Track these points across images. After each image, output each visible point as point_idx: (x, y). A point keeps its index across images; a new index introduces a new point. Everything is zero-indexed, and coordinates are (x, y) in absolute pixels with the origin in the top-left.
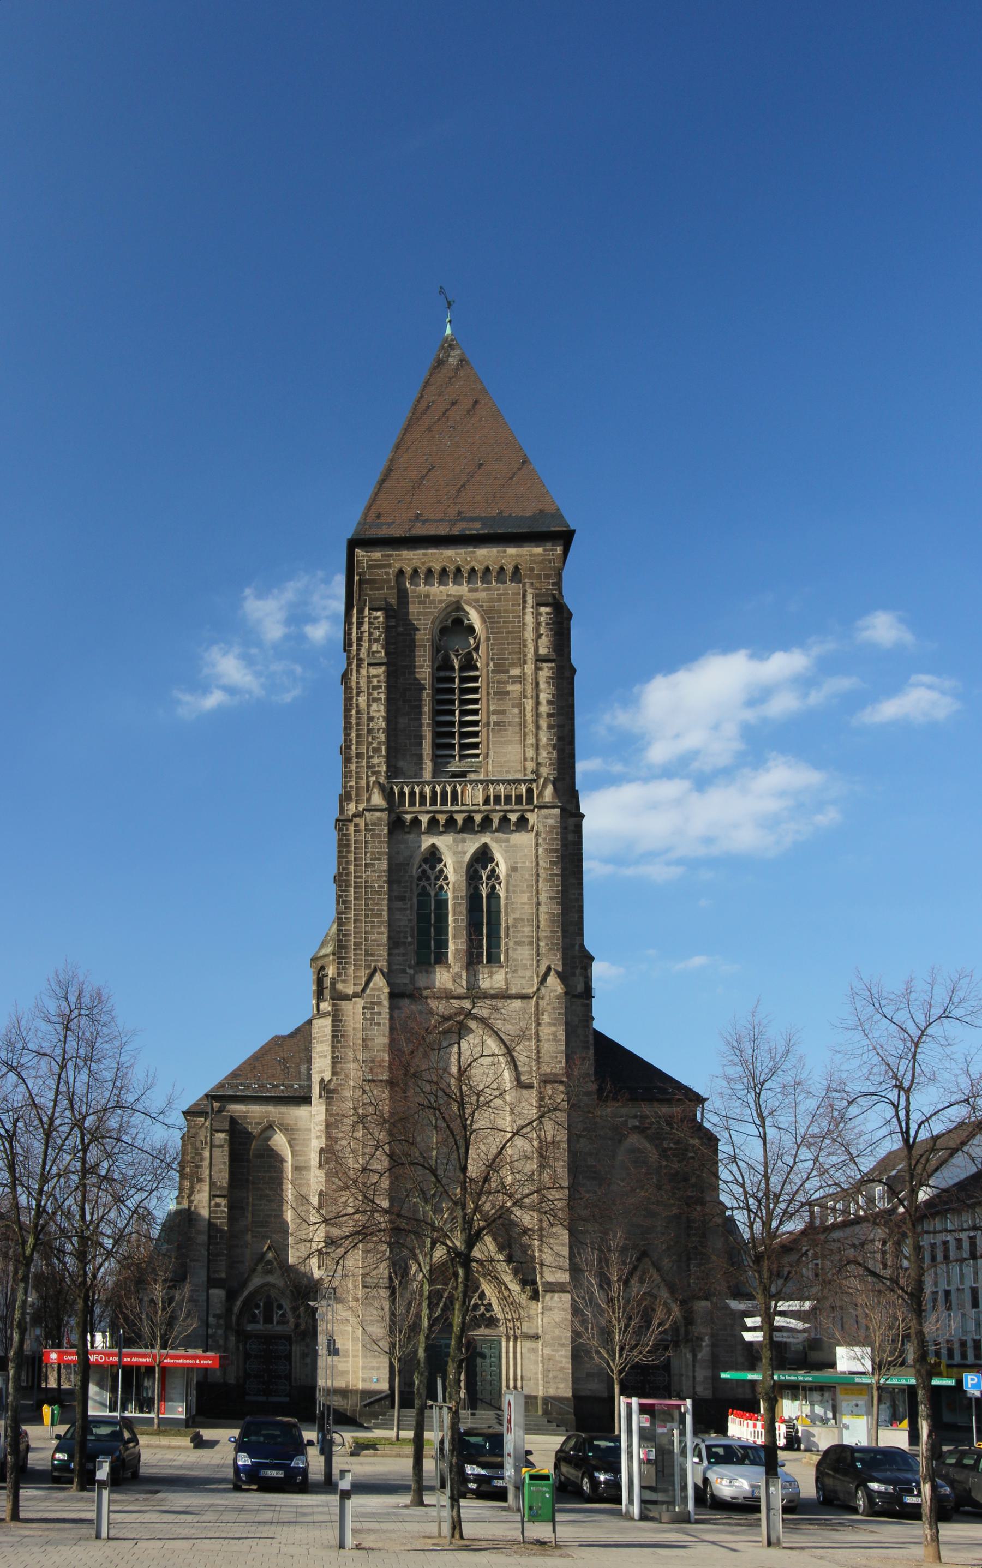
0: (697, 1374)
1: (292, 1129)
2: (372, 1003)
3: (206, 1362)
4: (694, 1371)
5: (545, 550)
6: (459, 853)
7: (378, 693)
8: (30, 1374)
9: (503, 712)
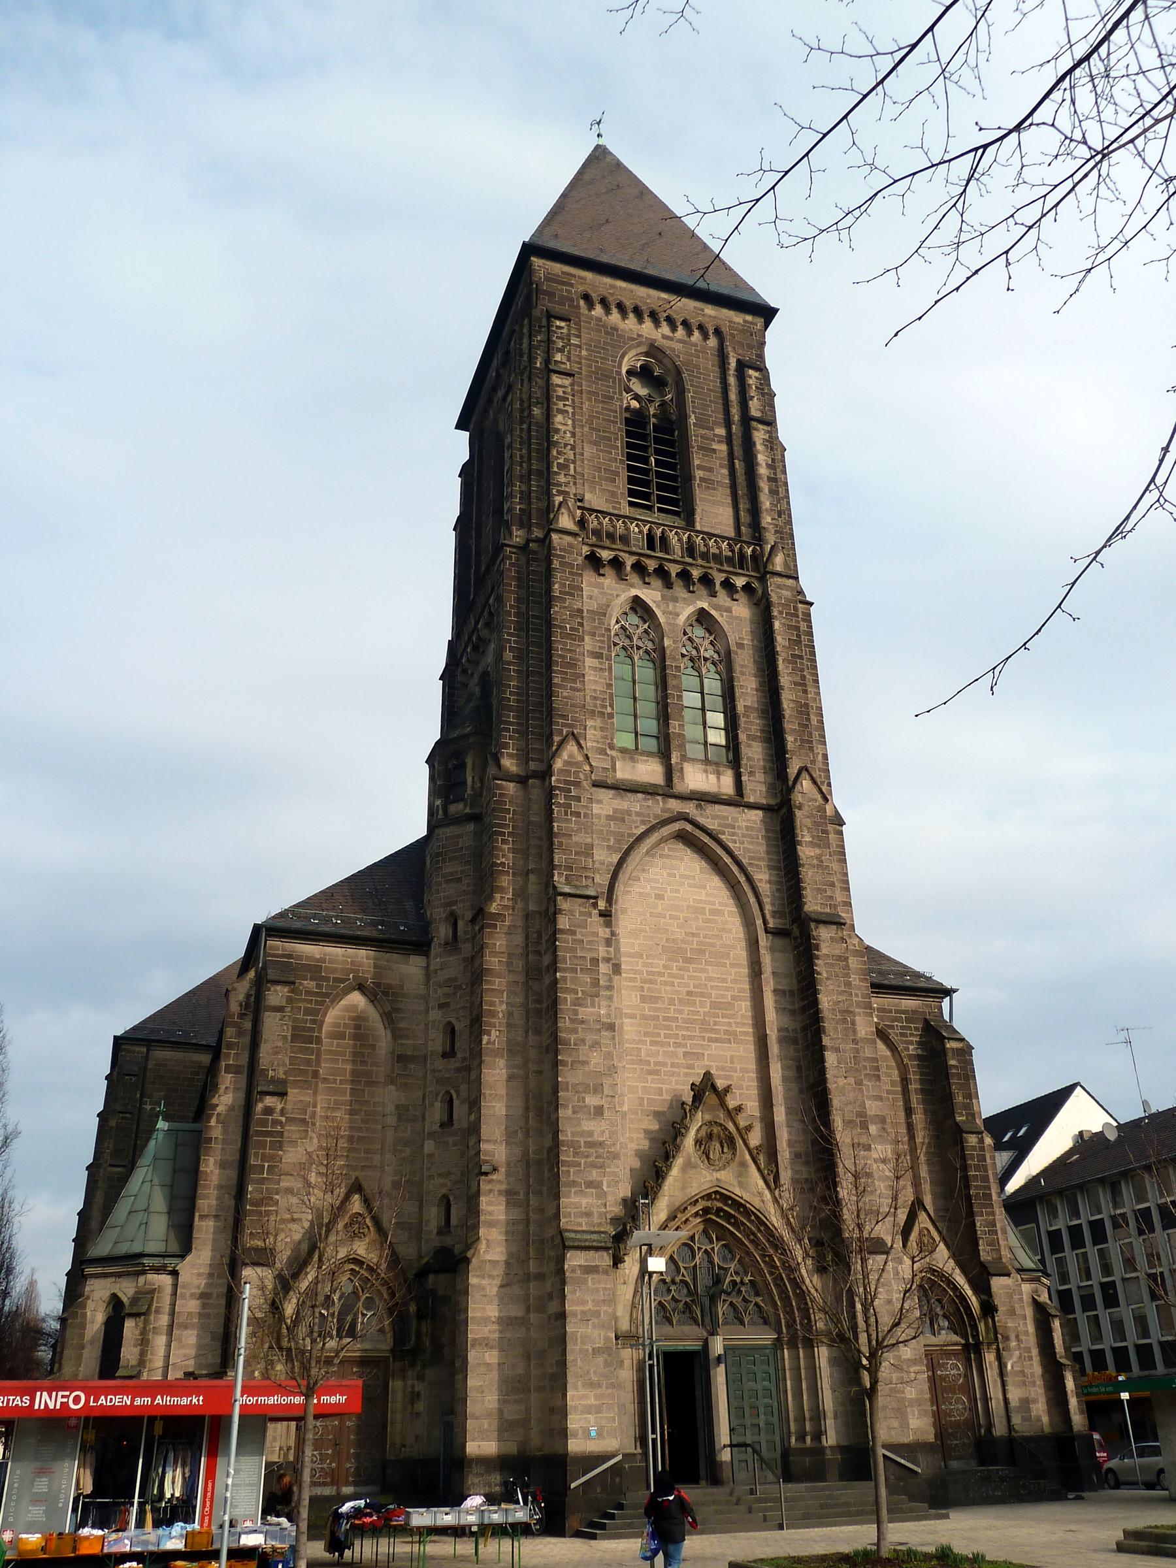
0: (1010, 1396)
1: (394, 994)
2: (567, 782)
3: (333, 1400)
4: (1004, 1392)
5: (745, 321)
6: (671, 613)
7: (565, 405)
8: (743, 505)
9: (710, 470)
